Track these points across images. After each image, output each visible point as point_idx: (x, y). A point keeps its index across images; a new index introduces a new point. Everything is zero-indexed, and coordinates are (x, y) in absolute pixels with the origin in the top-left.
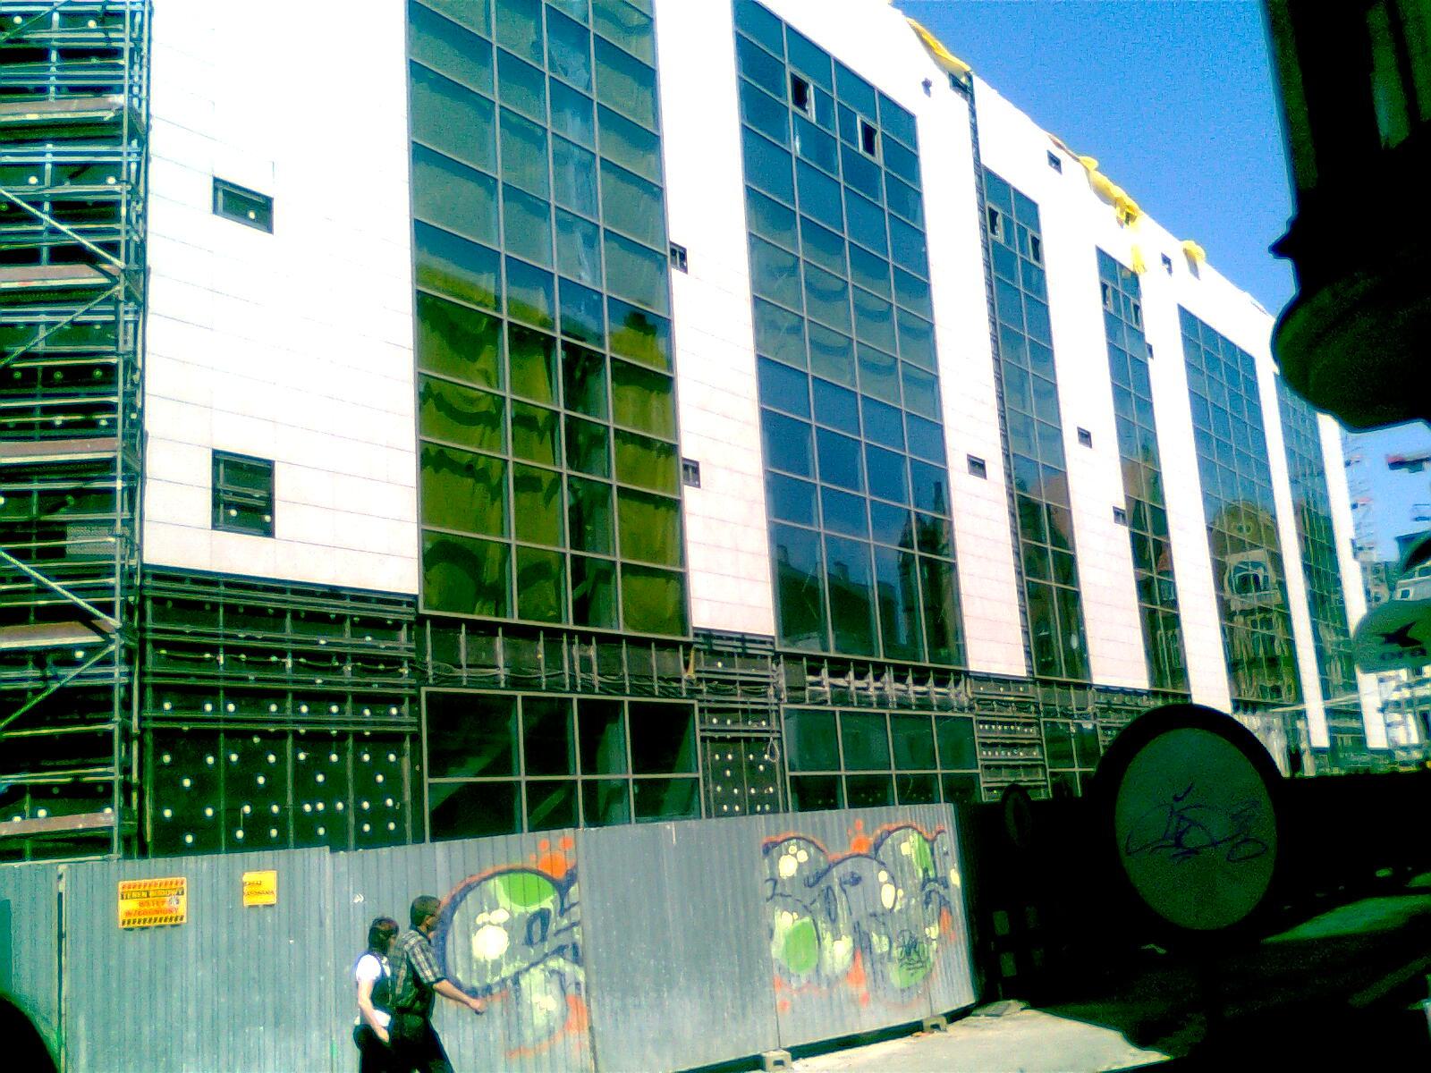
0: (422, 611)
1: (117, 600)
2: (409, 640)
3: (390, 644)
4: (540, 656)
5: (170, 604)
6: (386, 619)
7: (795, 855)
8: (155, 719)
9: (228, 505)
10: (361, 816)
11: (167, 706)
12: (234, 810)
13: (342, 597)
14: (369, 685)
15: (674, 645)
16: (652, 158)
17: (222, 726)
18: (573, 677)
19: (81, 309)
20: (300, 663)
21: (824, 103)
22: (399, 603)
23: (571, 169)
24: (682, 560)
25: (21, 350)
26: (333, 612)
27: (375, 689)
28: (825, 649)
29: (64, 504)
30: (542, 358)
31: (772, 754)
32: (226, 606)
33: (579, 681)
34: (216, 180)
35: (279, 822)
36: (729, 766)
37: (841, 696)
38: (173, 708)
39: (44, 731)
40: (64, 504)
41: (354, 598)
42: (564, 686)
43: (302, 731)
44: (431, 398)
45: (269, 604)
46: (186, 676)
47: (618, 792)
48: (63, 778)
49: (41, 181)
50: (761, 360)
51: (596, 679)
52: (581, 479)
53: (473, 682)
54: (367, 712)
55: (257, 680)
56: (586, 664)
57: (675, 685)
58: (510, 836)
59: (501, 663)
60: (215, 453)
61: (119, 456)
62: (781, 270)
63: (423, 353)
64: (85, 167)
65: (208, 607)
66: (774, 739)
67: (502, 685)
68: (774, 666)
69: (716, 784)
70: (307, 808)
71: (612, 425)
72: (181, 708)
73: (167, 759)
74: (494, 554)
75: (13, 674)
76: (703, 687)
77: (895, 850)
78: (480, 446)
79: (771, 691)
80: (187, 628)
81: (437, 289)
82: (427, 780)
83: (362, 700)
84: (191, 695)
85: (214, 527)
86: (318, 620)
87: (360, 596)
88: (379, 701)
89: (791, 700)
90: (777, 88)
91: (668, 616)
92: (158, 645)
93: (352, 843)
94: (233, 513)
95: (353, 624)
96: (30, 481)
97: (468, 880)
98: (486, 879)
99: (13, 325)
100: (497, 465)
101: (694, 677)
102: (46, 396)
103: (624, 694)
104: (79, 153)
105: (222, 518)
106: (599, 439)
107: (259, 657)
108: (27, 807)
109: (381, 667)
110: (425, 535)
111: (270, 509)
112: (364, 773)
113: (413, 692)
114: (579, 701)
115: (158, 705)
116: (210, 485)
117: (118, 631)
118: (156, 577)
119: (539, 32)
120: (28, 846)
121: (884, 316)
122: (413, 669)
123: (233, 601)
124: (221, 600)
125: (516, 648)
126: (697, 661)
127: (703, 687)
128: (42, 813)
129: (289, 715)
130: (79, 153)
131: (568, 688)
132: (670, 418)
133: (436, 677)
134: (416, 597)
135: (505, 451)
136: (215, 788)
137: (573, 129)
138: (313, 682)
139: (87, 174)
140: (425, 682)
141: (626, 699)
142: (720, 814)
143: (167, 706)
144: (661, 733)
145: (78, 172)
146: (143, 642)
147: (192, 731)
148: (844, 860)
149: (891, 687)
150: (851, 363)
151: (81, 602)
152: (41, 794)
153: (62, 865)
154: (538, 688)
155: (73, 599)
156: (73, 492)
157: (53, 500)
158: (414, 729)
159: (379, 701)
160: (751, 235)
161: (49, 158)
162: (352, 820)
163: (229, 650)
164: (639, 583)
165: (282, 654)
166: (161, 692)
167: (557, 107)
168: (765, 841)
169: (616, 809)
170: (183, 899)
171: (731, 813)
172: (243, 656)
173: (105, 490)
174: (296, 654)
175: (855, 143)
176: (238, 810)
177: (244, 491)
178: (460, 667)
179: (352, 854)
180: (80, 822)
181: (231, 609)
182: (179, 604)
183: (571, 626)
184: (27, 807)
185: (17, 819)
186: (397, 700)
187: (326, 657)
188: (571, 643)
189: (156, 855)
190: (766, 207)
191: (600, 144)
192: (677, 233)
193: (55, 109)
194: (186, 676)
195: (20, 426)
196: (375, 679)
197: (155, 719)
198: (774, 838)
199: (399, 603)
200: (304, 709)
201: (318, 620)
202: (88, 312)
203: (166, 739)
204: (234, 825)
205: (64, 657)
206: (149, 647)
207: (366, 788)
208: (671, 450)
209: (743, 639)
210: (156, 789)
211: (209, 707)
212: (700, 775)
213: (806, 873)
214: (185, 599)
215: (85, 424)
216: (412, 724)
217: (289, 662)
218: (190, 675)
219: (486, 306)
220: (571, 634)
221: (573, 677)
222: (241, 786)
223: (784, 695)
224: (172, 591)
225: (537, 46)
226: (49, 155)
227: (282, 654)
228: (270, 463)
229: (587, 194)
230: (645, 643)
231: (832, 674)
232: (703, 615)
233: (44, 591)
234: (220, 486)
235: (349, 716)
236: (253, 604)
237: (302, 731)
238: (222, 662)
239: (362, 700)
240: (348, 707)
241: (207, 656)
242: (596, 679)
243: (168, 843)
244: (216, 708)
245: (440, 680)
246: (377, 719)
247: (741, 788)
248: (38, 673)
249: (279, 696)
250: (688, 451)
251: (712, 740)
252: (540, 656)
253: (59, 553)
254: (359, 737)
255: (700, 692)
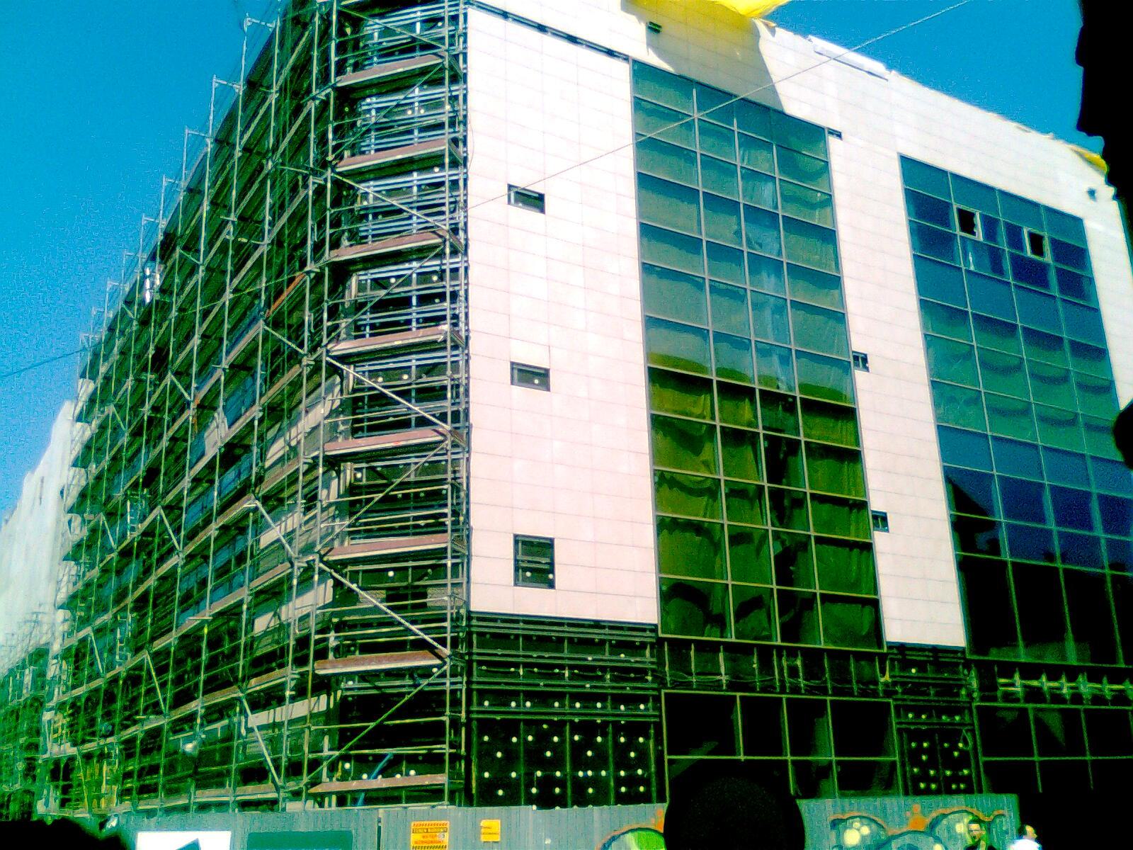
0: (661, 635)
1: (449, 636)
2: (652, 656)
3: (638, 659)
4: (755, 666)
5: (488, 636)
6: (635, 642)
7: (858, 830)
8: (478, 712)
9: (525, 569)
10: (620, 782)
11: (486, 703)
12: (530, 774)
13: (604, 627)
14: (624, 688)
15: (869, 657)
16: (836, 292)
17: (522, 717)
18: (782, 681)
19: (432, 453)
20: (574, 674)
21: (990, 225)
22: (644, 630)
23: (767, 313)
24: (875, 589)
25: (398, 481)
26: (597, 638)
27: (628, 691)
28: (1064, 657)
29: (426, 574)
30: (750, 448)
31: (966, 743)
32: (525, 637)
33: (788, 685)
34: (512, 363)
35: (561, 783)
36: (925, 751)
37: (1034, 695)
38: (490, 705)
39: (408, 721)
40: (426, 574)
41: (611, 628)
42: (775, 688)
43: (577, 720)
44: (663, 482)
45: (553, 634)
46: (499, 684)
47: (825, 771)
48: (422, 750)
49: (410, 377)
50: (941, 430)
51: (802, 682)
52: (788, 533)
53: (702, 686)
54: (622, 707)
55: (591, 687)
56: (793, 672)
57: (872, 687)
58: (647, 805)
59: (723, 671)
60: (516, 536)
61: (449, 545)
62: (957, 357)
63: (657, 455)
64: (435, 365)
65: (512, 637)
66: (967, 731)
67: (724, 688)
68: (966, 672)
69: (913, 765)
70: (581, 774)
71: (808, 491)
72: (494, 705)
73: (486, 738)
74: (718, 593)
75: (398, 683)
76: (899, 689)
77: (950, 829)
78: (704, 517)
79: (963, 692)
80: (499, 652)
81: (667, 411)
82: (667, 757)
83: (618, 699)
84: (502, 697)
85: (516, 585)
86: (587, 644)
87: (616, 626)
88: (632, 700)
89: (983, 699)
90: (946, 222)
91: (864, 633)
92: (480, 663)
93: (612, 800)
94: (528, 574)
95: (611, 645)
96: (407, 561)
97: (613, 834)
98: (623, 834)
99: (398, 465)
100: (718, 527)
101: (890, 680)
102: (416, 508)
103: (826, 694)
104: (429, 358)
105: (521, 578)
106: (799, 502)
107: (547, 670)
108: (404, 769)
109: (632, 675)
110: (661, 581)
111: (552, 571)
112: (622, 751)
113: (655, 693)
114: (788, 700)
115: (480, 704)
116: (512, 556)
117: (449, 656)
118: (479, 619)
119: (739, 224)
120: (404, 794)
121: (1065, 379)
122: (655, 677)
123: (572, 635)
124: (520, 632)
125: (734, 660)
126: (892, 669)
127: (899, 689)
128: (412, 772)
129: (567, 709)
130: (429, 358)
131: (778, 690)
132: (860, 481)
133: (673, 682)
134: (656, 625)
135: (723, 519)
136: (518, 758)
137: (768, 285)
138: (584, 687)
139: (436, 371)
140: (664, 685)
141: (829, 698)
142: (918, 792)
143: (486, 703)
144: (862, 728)
145: (430, 369)
146: (470, 663)
147: (502, 720)
148: (901, 835)
149: (1086, 687)
150: (1032, 421)
151: (427, 638)
152: (412, 760)
153: (382, 810)
154: (753, 690)
155: (422, 635)
156: (431, 566)
157: (421, 572)
158: (657, 720)
159: (632, 700)
160: (926, 336)
161: (414, 363)
162: (612, 784)
163: (526, 665)
164: (837, 609)
165: (562, 667)
166: (482, 694)
167: (754, 271)
168: (832, 818)
169: (825, 785)
170: (447, 835)
171: (927, 792)
172: (536, 670)
173: (446, 565)
174: (572, 667)
175: (1021, 248)
176: (532, 774)
177: (535, 560)
178: (691, 674)
179: (613, 807)
180: (428, 780)
181: (527, 638)
182: (494, 635)
183: (779, 643)
184: (404, 769)
185: (398, 776)
186: (644, 699)
187: (593, 669)
188: (780, 657)
189: (479, 805)
190: (939, 311)
191: (790, 291)
192: (858, 344)
193: (416, 335)
194: (499, 684)
195: (401, 528)
196: (628, 685)
197: (478, 712)
198: (840, 816)
199: (644, 630)
200: (578, 705)
201: (587, 644)
202: (435, 455)
203: (485, 726)
204: (529, 785)
205: (426, 672)
206: (475, 665)
207: (622, 762)
208: (863, 505)
209: (935, 650)
210: (480, 757)
211: (513, 704)
212: (897, 758)
213: (868, 842)
214: (501, 633)
215: (436, 526)
216: (655, 716)
217: (567, 673)
218: (502, 684)
219: (704, 418)
220: (779, 649)
221: (782, 681)
222: (534, 758)
223: (975, 695)
224: (489, 628)
225: (738, 233)
226: (414, 361)
227: (562, 667)
228: (552, 540)
229: (780, 330)
230: (845, 655)
231: (1022, 677)
232: (894, 632)
233: (408, 631)
234: (520, 557)
235: (609, 710)
236: (544, 636)
237: (577, 720)
238: (521, 673)
239: (618, 699)
240: (609, 704)
241: (512, 669)
242: (802, 682)
243: (487, 797)
244: (518, 706)
245: (676, 684)
246: (630, 712)
247: (936, 769)
248: (411, 683)
249: (560, 696)
250: (876, 504)
251: (907, 730)
252: (755, 666)
253: (423, 606)
254: (616, 724)
255: (896, 692)
